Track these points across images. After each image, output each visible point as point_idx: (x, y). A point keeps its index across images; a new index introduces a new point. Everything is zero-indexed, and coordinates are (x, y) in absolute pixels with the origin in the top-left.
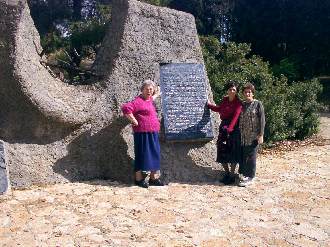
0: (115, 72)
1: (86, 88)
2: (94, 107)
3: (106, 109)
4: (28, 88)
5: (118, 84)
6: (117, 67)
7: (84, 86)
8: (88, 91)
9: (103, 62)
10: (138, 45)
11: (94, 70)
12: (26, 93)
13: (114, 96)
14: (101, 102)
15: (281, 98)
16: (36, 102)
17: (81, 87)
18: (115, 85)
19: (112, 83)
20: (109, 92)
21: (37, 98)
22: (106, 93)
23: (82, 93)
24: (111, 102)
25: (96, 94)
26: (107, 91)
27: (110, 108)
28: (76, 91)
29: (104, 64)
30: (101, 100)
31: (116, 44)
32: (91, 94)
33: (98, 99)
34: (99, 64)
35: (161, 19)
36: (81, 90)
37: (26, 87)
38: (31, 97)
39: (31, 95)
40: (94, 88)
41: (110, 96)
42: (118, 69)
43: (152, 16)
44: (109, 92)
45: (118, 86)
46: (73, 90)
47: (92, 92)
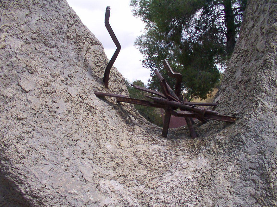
0: (263, 104)
1: (194, 146)
2: (206, 199)
3: (242, 201)
4: (14, 162)
5: (272, 135)
6: (266, 92)
7: (190, 140)
8: (196, 154)
9: (236, 83)
11: (217, 102)
12: (9, 173)
13: (261, 166)
14: (227, 184)
15: (196, 79)
16: (36, 197)
17: (184, 143)
18: (263, 136)
19: (255, 131)
20: (249, 157)
21: (39, 186)
22: (240, 158)
23: (183, 160)
24: (254, 181)
25: (216, 162)
26: (243, 155)
27: (254, 196)
28: (171, 154)
29: (236, 88)
30: (227, 178)
31: (260, 38)
32: (201, 162)
33: (220, 176)
34: (227, 88)
36: (183, 151)
37: (8, 160)
38: (22, 183)
39: (22, 177)
40: (212, 144)
41: (253, 167)
42: (269, 95)
44: (249, 157)
45: (273, 140)
46: (163, 150)
47: (205, 157)
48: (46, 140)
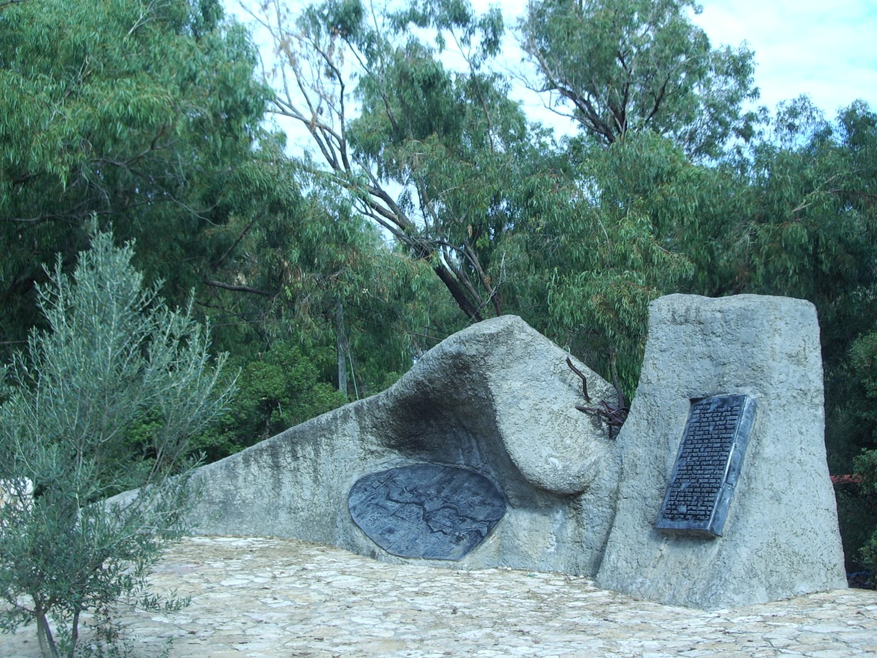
10: (660, 373)
35: (701, 323)
43: (686, 321)
48: (527, 435)
